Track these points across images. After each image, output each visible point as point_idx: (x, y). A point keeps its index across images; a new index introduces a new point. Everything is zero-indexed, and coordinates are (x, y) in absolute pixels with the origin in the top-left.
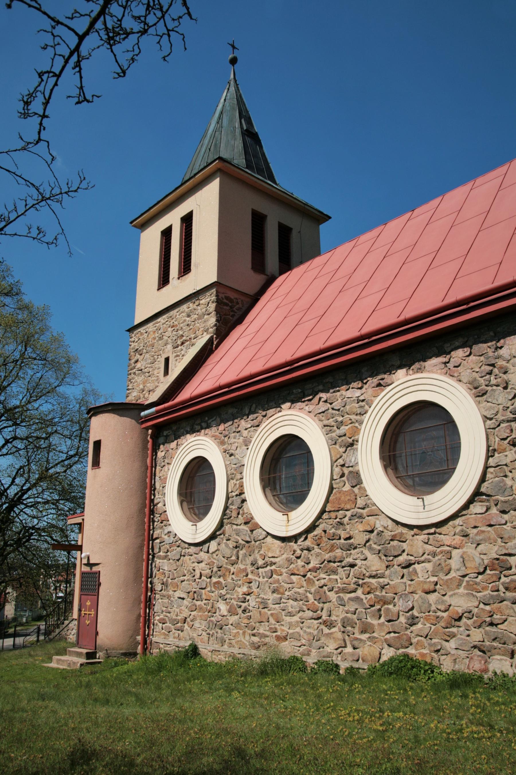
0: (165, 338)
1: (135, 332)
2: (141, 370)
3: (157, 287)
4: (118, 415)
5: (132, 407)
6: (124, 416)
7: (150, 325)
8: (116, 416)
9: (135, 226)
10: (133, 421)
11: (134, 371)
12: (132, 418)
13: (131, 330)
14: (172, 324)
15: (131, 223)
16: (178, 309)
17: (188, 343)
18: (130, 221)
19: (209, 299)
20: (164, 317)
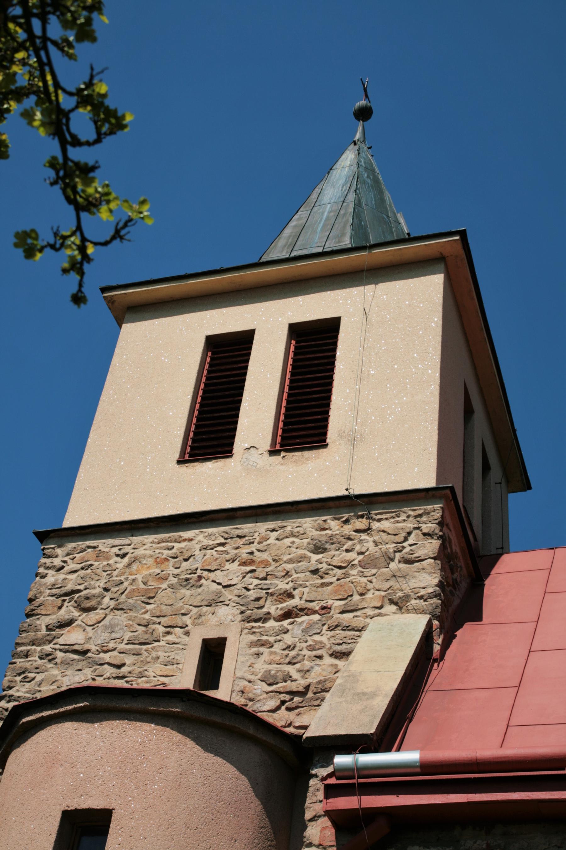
0: (208, 587)
1: (71, 546)
2: (84, 653)
3: (177, 456)
4: (197, 741)
5: (251, 731)
6: (217, 753)
7: (149, 539)
8: (190, 743)
9: (110, 302)
10: (244, 782)
11: (48, 648)
12: (242, 771)
13: (43, 536)
14: (245, 556)
15: (104, 290)
16: (279, 523)
17: (316, 617)
18: (103, 285)
19: (410, 525)
20: (210, 530)
